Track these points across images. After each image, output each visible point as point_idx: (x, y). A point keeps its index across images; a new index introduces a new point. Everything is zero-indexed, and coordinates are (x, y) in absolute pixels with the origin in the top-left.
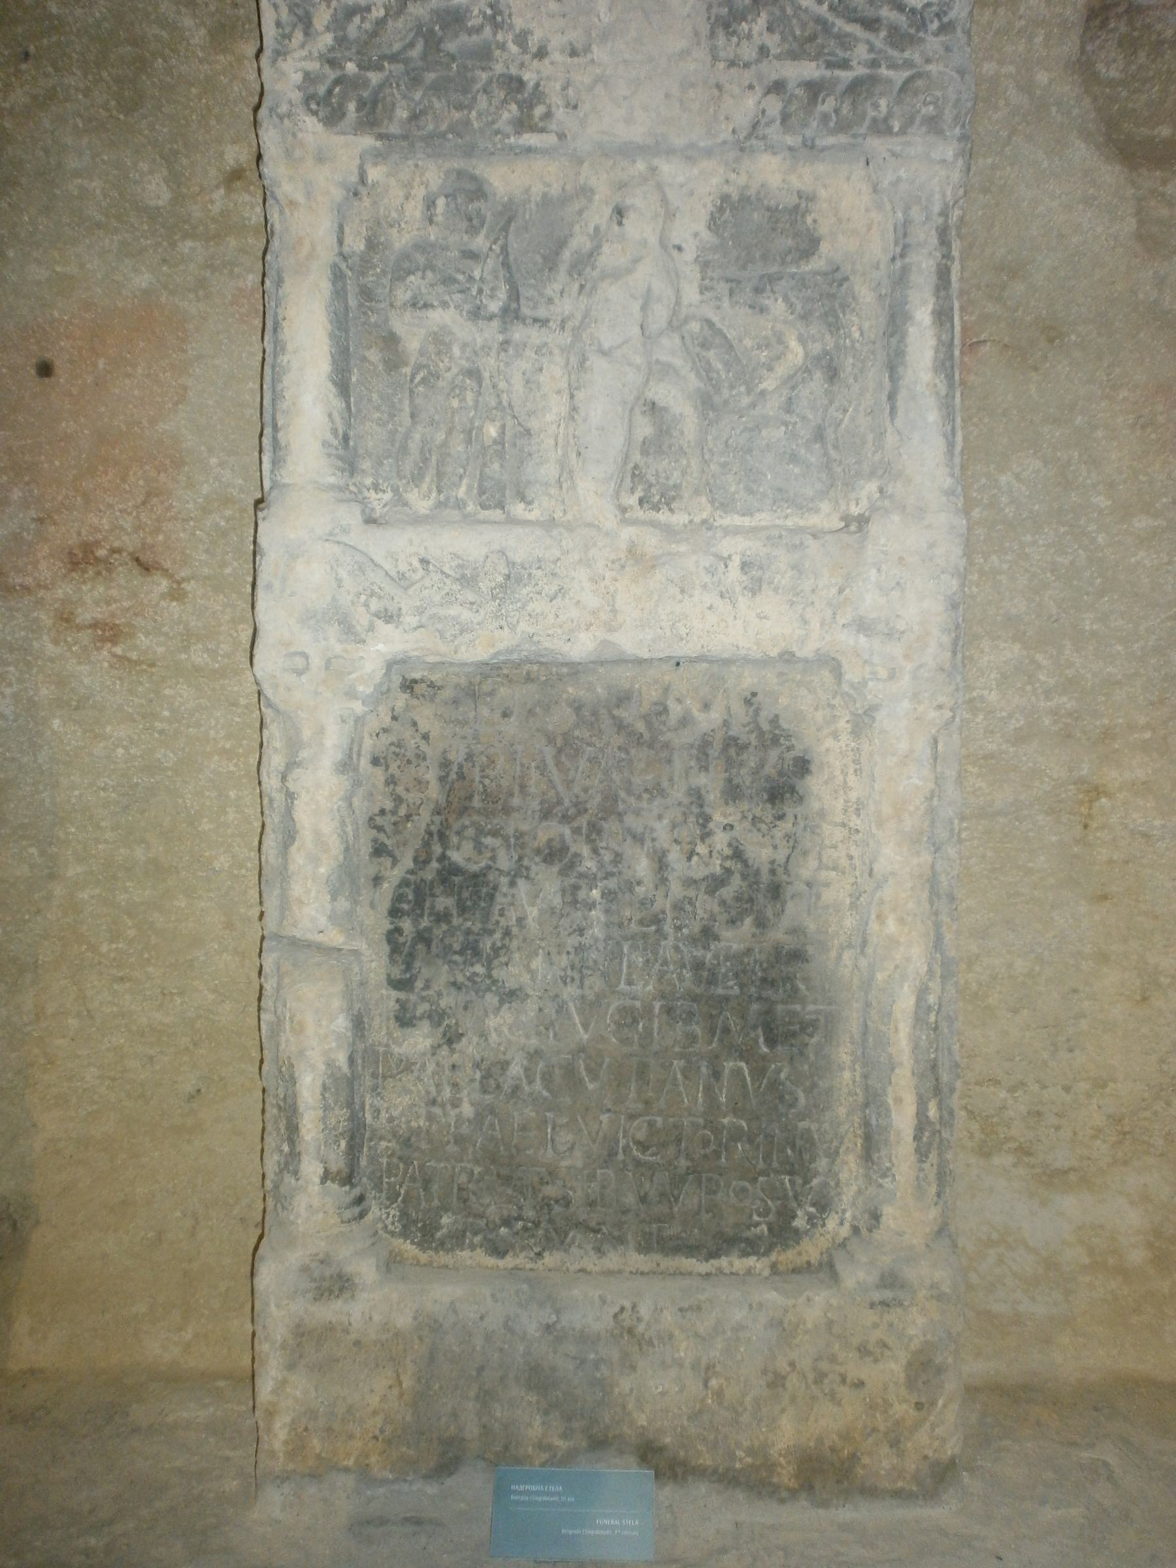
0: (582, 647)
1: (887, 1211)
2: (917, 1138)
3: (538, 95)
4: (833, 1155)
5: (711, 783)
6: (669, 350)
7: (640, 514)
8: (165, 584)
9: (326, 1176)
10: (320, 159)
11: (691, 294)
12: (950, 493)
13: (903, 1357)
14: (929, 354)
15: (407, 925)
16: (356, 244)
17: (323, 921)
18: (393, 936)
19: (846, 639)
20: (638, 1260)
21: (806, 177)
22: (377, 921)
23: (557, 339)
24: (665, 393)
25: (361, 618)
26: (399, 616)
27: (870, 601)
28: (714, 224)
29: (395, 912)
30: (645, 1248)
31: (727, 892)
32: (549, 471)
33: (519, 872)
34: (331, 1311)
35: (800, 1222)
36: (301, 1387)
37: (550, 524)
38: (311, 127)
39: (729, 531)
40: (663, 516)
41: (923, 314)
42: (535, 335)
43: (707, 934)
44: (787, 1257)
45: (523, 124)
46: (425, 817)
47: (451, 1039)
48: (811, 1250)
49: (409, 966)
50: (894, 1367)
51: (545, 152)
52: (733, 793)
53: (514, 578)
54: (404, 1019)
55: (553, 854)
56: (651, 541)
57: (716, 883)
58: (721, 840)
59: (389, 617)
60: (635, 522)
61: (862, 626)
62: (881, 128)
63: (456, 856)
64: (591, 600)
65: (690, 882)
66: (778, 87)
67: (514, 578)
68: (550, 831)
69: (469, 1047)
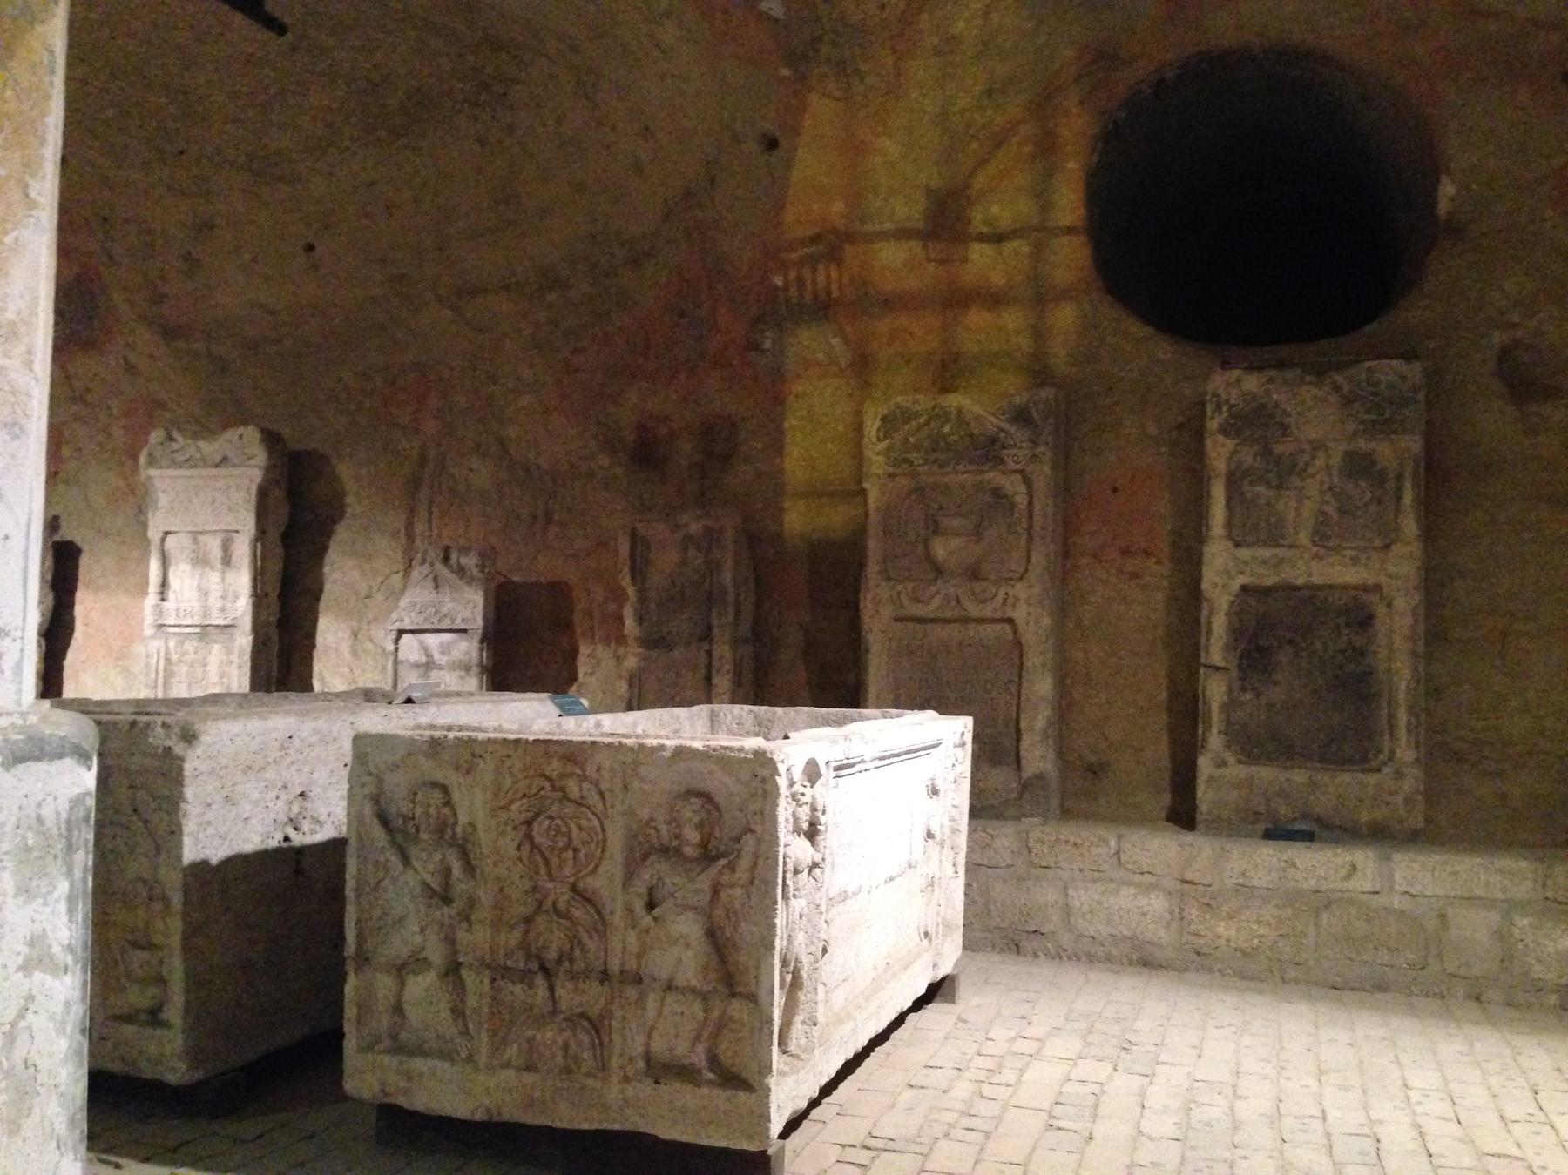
0: (1300, 581)
1: (1398, 750)
2: (1407, 728)
3: (1288, 427)
4: (1381, 736)
5: (1341, 621)
6: (1328, 497)
7: (1320, 543)
8: (1154, 560)
9: (1220, 732)
10: (1223, 446)
11: (1336, 480)
12: (1419, 536)
13: (1403, 796)
14: (1410, 498)
15: (1245, 662)
16: (1233, 468)
17: (1220, 659)
18: (1240, 665)
19: (1383, 579)
20: (1318, 765)
21: (1373, 444)
22: (1235, 661)
23: (1293, 493)
24: (1327, 508)
25: (1234, 573)
26: (1496, 932)
27: (1391, 569)
28: (1343, 460)
29: (1241, 657)
30: (1319, 762)
31: (1346, 655)
32: (1292, 531)
33: (1280, 647)
34: (1220, 771)
35: (1370, 756)
36: (1210, 795)
37: (1291, 546)
38: (1221, 438)
39: (1345, 548)
40: (1325, 543)
41: (1408, 485)
42: (1288, 493)
43: (1341, 667)
44: (1366, 766)
45: (1284, 435)
46: (1251, 630)
47: (1258, 695)
48: (1374, 764)
49: (1245, 673)
50: (1400, 799)
51: (1291, 442)
52: (1347, 625)
53: (1281, 561)
54: (1244, 690)
55: (1290, 642)
56: (1322, 551)
57: (1343, 652)
58: (1345, 638)
59: (1242, 573)
60: (1318, 545)
61: (1390, 576)
62: (1395, 432)
63: (1261, 642)
64: (1303, 568)
65: (1335, 651)
66: (1363, 422)
67: (1281, 561)
68: (1288, 636)
69: (1264, 700)
